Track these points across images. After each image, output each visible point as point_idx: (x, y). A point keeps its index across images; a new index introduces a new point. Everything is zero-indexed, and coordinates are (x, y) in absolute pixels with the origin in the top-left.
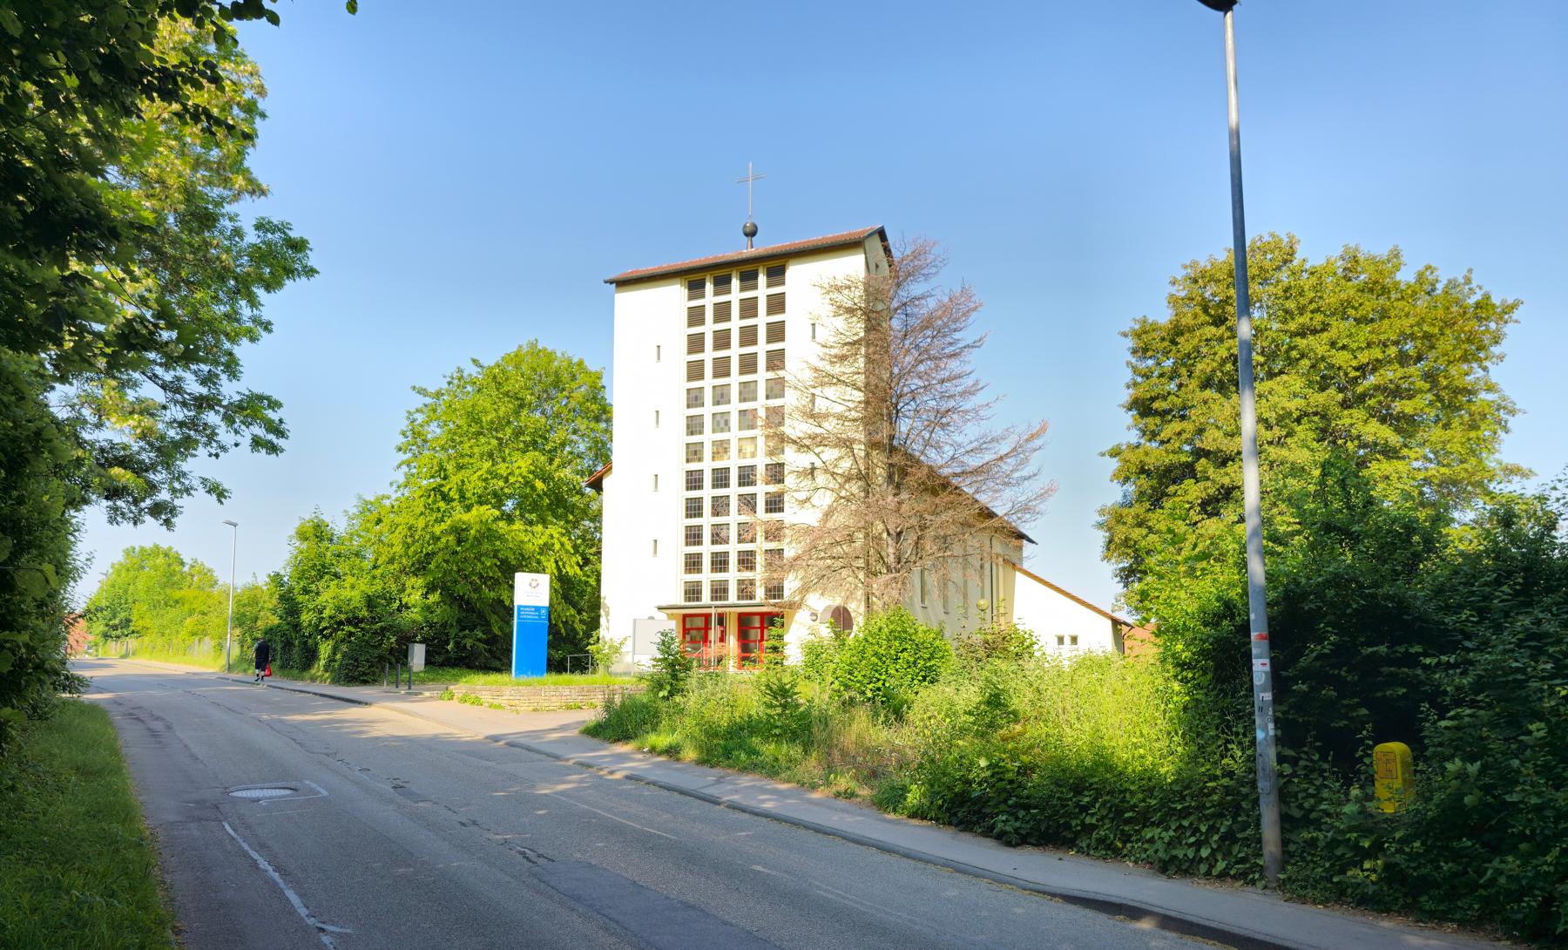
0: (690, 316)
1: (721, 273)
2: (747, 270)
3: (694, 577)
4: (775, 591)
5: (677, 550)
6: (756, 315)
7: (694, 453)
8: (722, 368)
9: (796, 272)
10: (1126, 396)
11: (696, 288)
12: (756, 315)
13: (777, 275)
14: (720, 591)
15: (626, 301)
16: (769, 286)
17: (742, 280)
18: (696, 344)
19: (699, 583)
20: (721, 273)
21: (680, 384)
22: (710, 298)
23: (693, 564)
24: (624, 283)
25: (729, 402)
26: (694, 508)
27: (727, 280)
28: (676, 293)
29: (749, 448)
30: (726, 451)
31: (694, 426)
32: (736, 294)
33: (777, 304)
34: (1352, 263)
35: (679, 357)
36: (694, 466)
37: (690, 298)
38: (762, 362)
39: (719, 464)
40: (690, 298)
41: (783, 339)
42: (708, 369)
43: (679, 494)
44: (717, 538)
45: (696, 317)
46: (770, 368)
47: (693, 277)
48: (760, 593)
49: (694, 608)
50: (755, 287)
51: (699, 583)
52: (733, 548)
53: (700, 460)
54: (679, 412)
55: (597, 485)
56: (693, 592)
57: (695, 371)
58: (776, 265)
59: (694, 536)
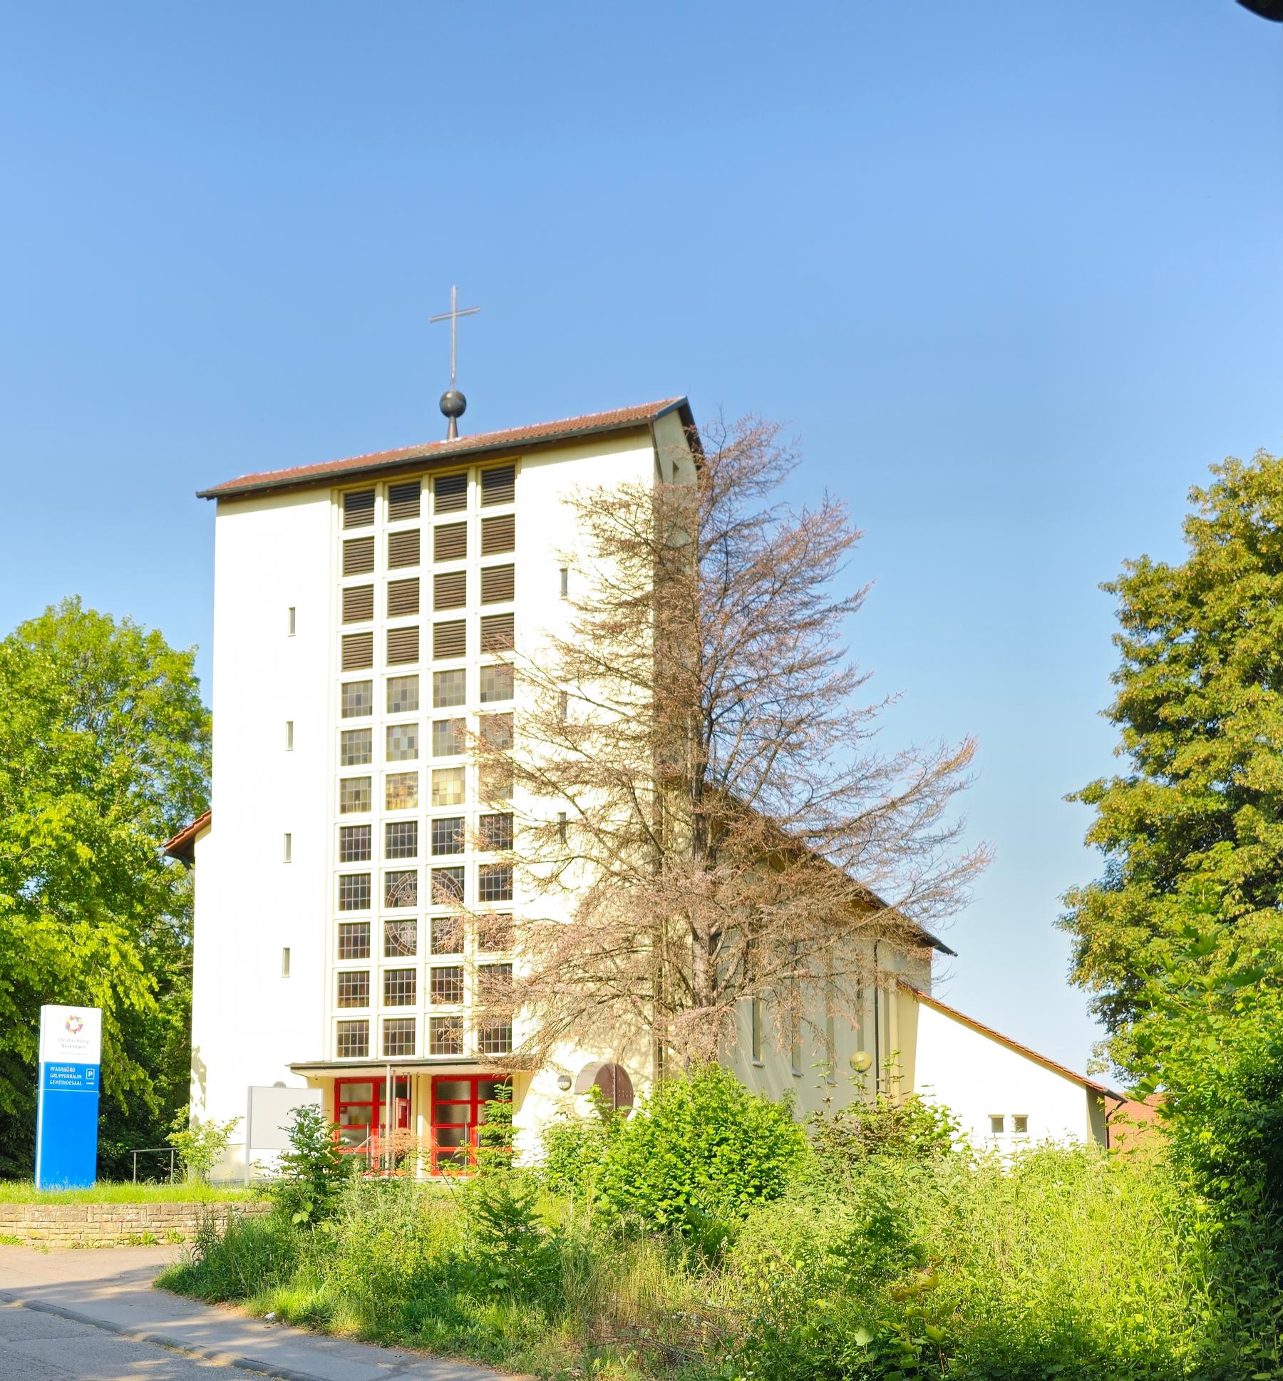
1: (401, 480)
2: (448, 475)
3: (354, 1013)
5: (325, 965)
9: (533, 479)
11: (358, 507)
15: (235, 527)
17: (439, 492)
20: (401, 480)
23: (353, 989)
24: (231, 498)
27: (414, 493)
28: (323, 515)
29: (450, 787)
33: (500, 535)
37: (348, 524)
43: (331, 868)
47: (353, 488)
49: (354, 1065)
52: (423, 963)
56: (353, 1039)
58: (498, 466)
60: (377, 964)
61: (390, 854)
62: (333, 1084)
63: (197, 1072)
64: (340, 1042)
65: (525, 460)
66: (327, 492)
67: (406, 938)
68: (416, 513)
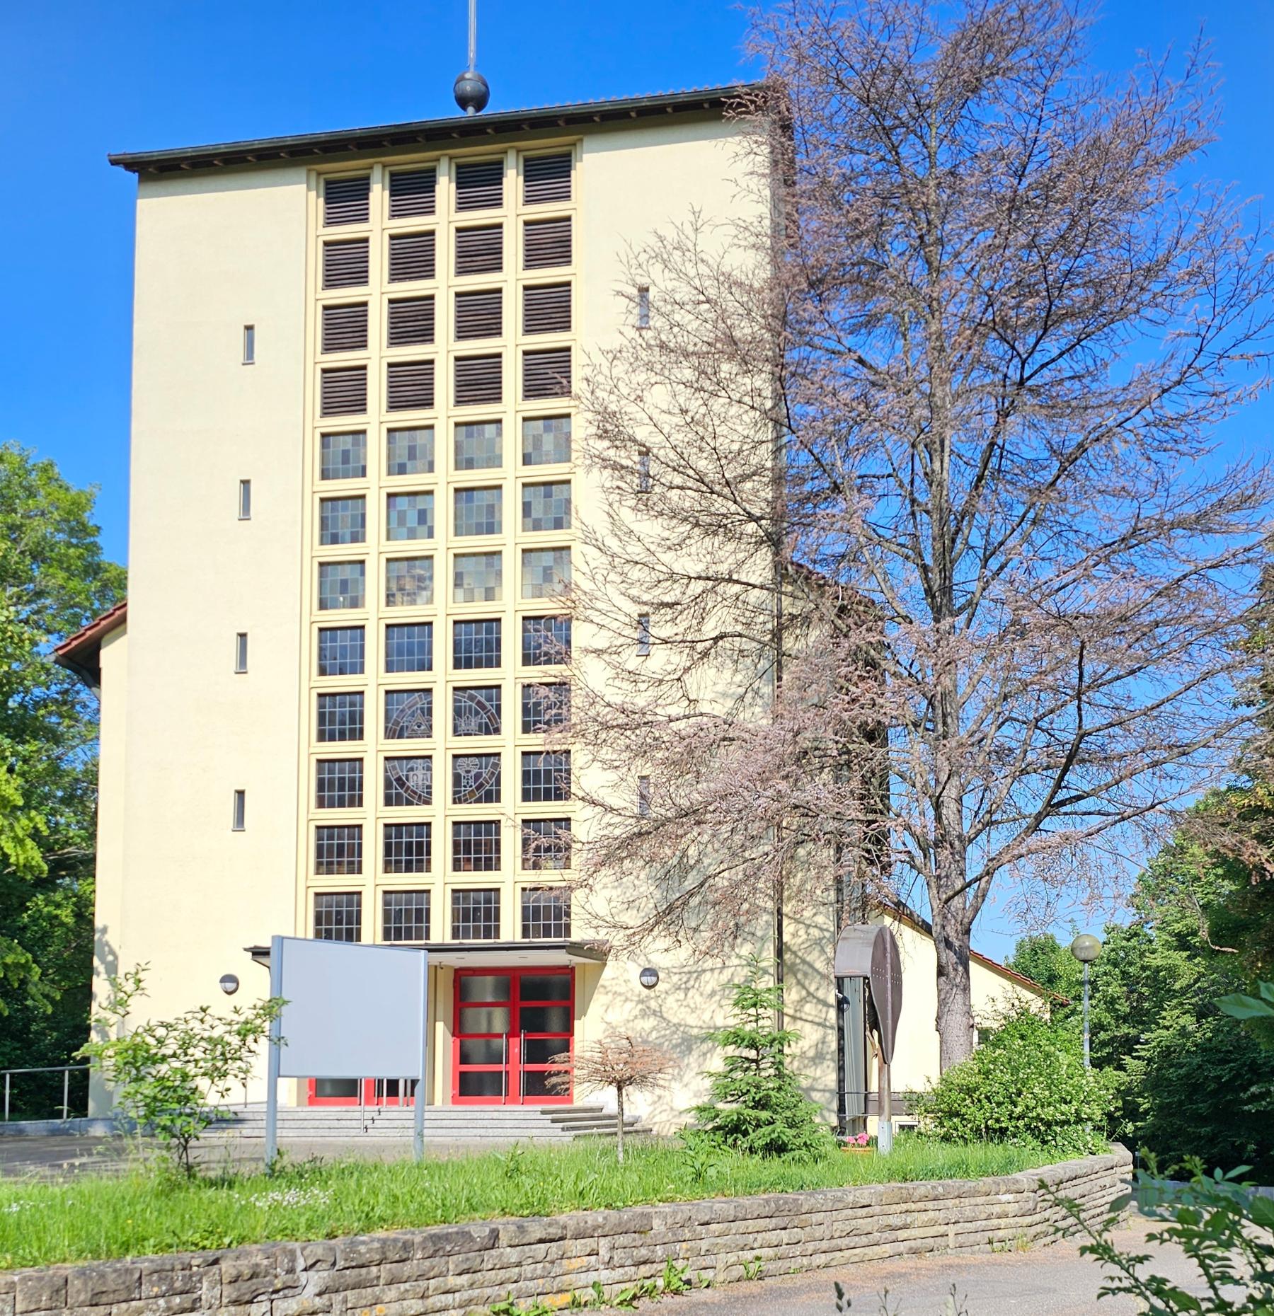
0: (329, 264)
3: (340, 882)
4: (546, 916)
5: (289, 815)
6: (430, 274)
7: (338, 584)
8: (411, 387)
10: (200, 1089)
11: (345, 197)
12: (430, 274)
13: (550, 174)
16: (463, 205)
18: (344, 327)
19: (354, 897)
21: (304, 417)
22: (380, 223)
24: (162, 170)
25: (363, 473)
26: (338, 718)
30: (425, 582)
31: (339, 519)
32: (446, 215)
33: (550, 243)
34: (1020, 946)
35: (299, 356)
36: (340, 617)
37: (329, 222)
38: (512, 376)
39: (405, 613)
40: (329, 222)
41: (566, 325)
42: (377, 388)
44: (397, 791)
45: (344, 264)
46: (533, 390)
48: (510, 927)
50: (496, 201)
51: (354, 897)
52: (441, 814)
53: (355, 603)
54: (294, 489)
55: (84, 664)
57: (343, 392)
58: (546, 144)
59: (338, 784)
60: (373, 816)
63: (103, 961)
64: (318, 921)
65: (588, 142)
66: (302, 172)
67: (415, 781)
68: (497, 202)
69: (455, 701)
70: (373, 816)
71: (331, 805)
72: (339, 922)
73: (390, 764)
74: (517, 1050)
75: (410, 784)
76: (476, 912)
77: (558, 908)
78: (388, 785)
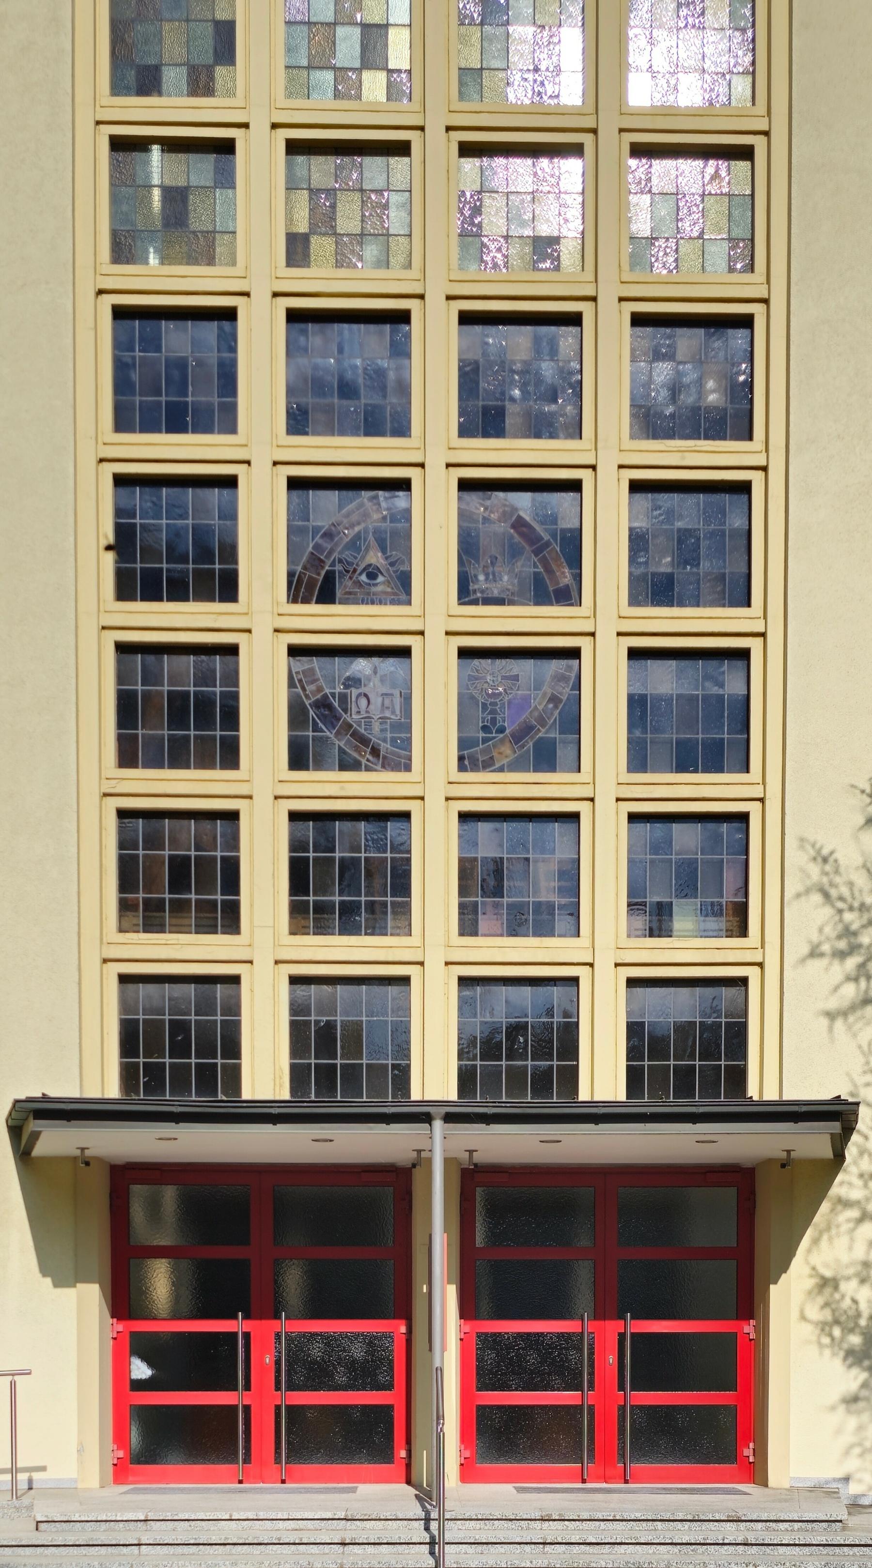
4: (695, 1052)
14: (343, 1055)
23: (174, 872)
56: (176, 1046)
61: (298, 422)
62: (98, 1188)
67: (369, 710)
69: (119, 512)
70: (263, 791)
71: (155, 763)
72: (180, 1049)
73: (301, 990)
74: (612, 1359)
75: (353, 718)
76: (523, 1052)
77: (206, 1030)
78: (297, 715)
